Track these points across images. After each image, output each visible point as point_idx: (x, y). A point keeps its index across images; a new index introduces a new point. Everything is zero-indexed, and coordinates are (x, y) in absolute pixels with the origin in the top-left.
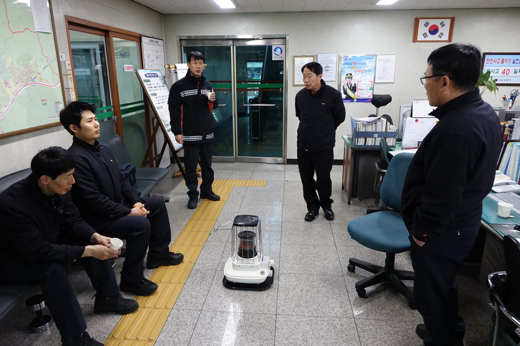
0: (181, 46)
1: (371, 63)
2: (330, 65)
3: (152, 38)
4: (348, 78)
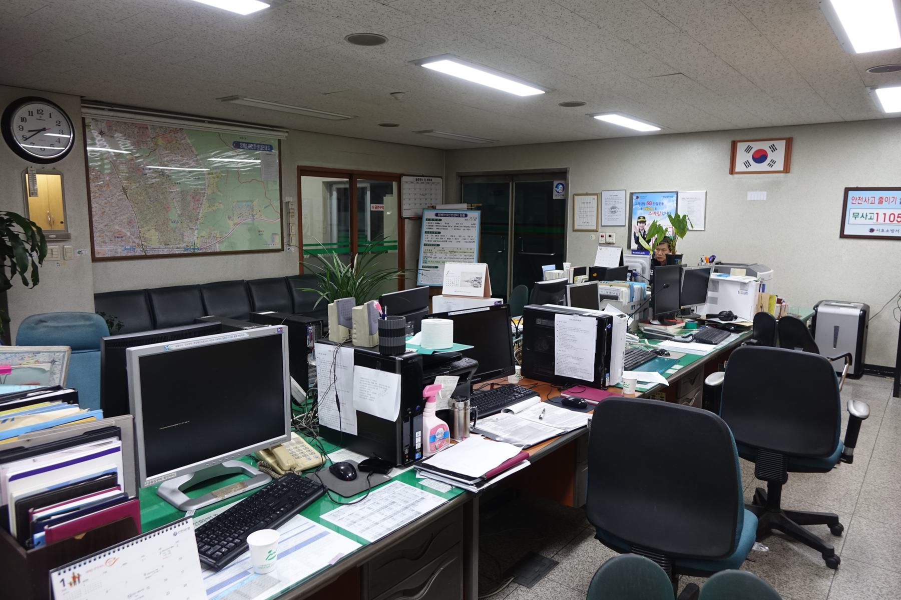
0: (461, 183)
1: (670, 204)
2: (617, 205)
4: (640, 222)
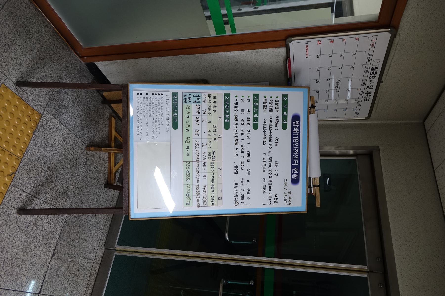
3: (380, 81)
